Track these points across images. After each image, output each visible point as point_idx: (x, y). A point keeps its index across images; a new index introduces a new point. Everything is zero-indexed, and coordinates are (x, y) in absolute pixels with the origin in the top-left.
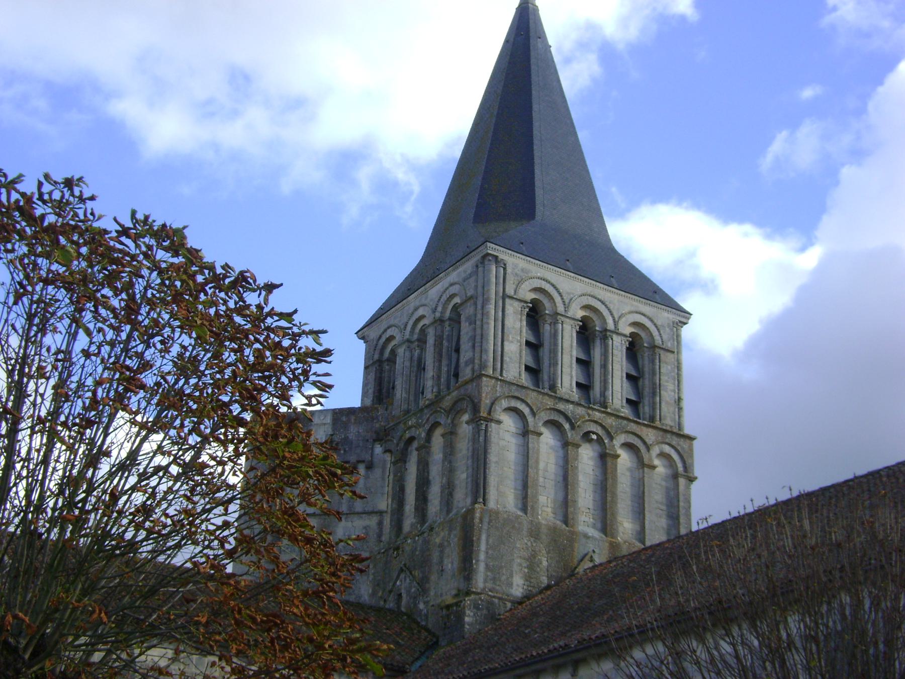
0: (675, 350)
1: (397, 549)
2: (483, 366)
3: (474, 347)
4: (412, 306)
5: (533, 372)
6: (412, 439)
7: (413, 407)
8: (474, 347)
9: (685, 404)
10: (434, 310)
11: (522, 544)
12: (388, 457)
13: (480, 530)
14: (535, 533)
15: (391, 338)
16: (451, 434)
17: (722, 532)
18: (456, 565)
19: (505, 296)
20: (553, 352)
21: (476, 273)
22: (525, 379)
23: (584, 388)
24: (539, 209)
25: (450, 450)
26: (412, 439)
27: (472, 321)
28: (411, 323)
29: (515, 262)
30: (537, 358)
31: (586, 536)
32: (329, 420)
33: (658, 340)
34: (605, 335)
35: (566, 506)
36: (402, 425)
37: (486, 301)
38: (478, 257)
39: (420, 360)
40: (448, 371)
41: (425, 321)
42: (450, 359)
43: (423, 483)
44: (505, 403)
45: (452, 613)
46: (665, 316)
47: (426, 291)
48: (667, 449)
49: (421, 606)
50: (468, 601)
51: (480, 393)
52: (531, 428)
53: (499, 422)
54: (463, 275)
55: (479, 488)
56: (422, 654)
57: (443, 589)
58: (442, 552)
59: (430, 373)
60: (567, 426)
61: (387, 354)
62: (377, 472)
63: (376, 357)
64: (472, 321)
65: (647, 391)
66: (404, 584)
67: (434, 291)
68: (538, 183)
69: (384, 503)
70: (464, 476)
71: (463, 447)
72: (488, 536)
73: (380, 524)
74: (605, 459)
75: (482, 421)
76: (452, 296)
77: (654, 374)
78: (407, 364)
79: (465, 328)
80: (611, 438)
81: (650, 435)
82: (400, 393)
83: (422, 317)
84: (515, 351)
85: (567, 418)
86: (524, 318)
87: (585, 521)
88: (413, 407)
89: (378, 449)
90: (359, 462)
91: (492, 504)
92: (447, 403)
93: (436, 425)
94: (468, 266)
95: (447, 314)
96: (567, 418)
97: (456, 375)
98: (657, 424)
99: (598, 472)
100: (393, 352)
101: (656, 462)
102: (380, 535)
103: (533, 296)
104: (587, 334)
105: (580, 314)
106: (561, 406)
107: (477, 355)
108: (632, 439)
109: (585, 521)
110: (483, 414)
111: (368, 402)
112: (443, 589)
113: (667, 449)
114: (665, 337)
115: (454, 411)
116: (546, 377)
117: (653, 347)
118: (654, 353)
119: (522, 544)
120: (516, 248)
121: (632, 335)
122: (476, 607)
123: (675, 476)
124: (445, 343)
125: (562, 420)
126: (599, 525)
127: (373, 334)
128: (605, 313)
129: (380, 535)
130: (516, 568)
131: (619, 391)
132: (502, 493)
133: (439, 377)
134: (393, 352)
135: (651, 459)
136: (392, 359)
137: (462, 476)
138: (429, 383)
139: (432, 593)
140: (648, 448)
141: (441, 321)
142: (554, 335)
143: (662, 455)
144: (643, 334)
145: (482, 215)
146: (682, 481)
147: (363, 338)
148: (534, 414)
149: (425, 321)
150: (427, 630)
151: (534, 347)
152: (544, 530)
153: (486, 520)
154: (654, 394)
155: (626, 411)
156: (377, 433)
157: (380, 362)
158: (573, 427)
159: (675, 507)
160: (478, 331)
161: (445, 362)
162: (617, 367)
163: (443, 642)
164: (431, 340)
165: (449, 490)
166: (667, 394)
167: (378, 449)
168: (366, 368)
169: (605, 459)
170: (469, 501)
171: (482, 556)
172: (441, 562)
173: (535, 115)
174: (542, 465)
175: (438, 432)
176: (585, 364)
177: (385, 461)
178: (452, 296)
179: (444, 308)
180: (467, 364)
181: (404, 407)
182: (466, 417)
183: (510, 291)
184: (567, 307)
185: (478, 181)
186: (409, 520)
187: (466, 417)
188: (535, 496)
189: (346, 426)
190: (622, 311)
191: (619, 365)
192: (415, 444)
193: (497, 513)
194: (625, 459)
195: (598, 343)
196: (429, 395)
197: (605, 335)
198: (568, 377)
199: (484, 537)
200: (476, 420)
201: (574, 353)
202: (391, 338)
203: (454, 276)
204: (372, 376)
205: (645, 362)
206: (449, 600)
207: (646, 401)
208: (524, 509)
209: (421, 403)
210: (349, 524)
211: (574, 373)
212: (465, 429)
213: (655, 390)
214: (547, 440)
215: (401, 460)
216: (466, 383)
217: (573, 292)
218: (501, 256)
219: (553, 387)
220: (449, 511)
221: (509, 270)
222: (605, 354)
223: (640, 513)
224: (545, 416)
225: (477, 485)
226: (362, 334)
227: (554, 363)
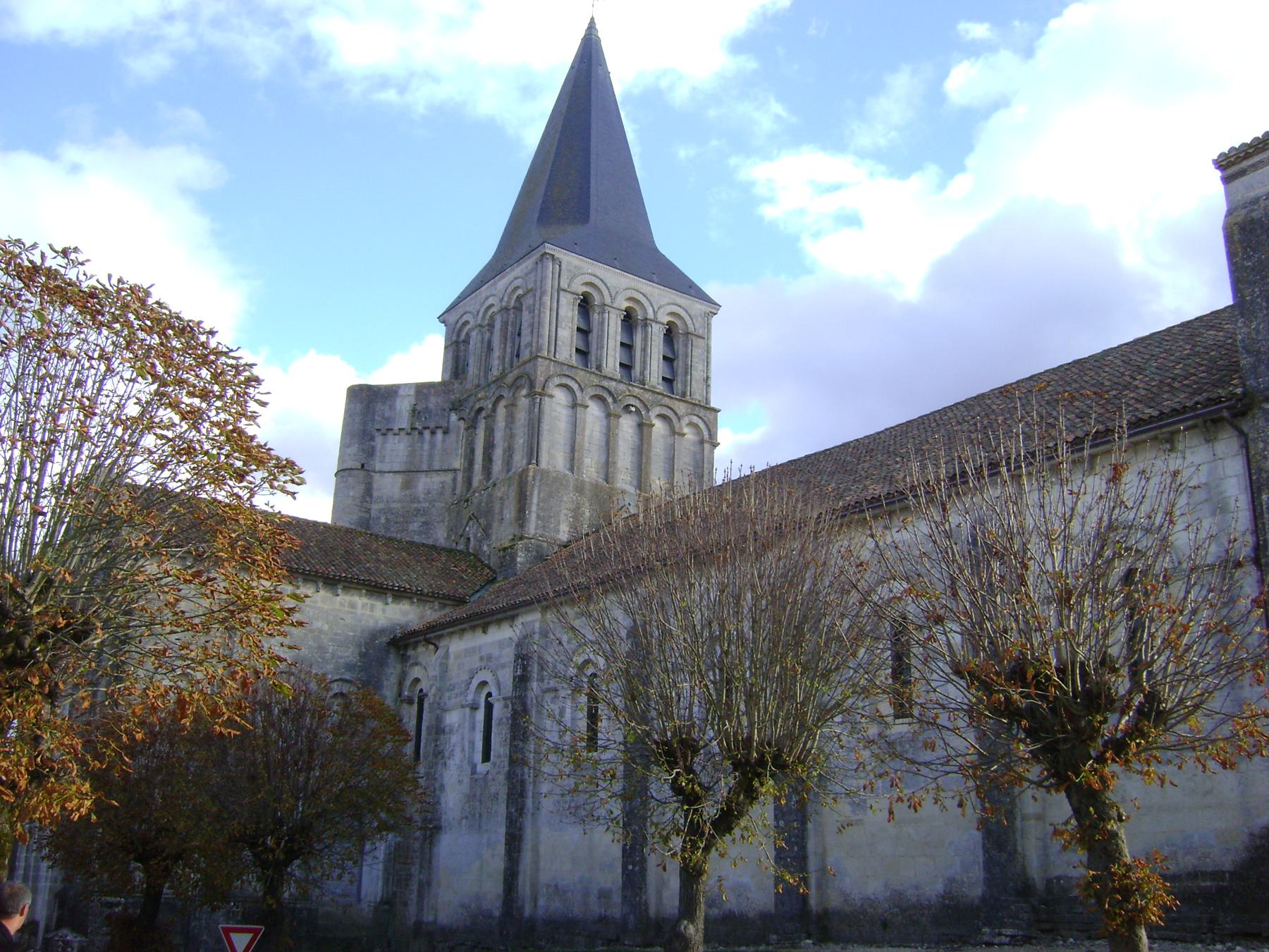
0: (706, 337)
1: (467, 501)
2: (539, 349)
3: (532, 332)
4: (484, 296)
5: (583, 353)
6: (481, 409)
7: (483, 382)
8: (532, 332)
9: (713, 382)
10: (502, 300)
11: (568, 499)
12: (462, 424)
13: (533, 486)
14: (579, 489)
15: (467, 323)
16: (512, 405)
17: (739, 486)
18: (513, 515)
19: (559, 289)
20: (601, 337)
21: (536, 269)
22: (574, 360)
23: (626, 367)
24: (592, 217)
25: (511, 419)
26: (481, 409)
27: (532, 311)
28: (482, 310)
29: (570, 260)
30: (587, 343)
31: (623, 492)
32: (412, 392)
33: (691, 329)
34: (646, 322)
36: (473, 398)
37: (543, 293)
38: (538, 255)
39: (490, 342)
40: (512, 352)
41: (494, 309)
42: (513, 343)
43: (489, 446)
44: (557, 381)
45: (507, 553)
47: (495, 284)
48: (695, 419)
49: (485, 548)
50: (520, 544)
51: (535, 371)
52: (579, 402)
53: (551, 396)
55: (533, 452)
56: (482, 587)
57: (502, 534)
58: (502, 504)
59: (497, 353)
60: (610, 400)
61: (463, 334)
62: (452, 437)
63: (454, 338)
64: (532, 311)
65: (680, 371)
66: (472, 530)
67: (502, 283)
68: (593, 190)
69: (458, 463)
70: (521, 441)
71: (521, 416)
72: (539, 492)
74: (643, 427)
75: (537, 395)
76: (516, 288)
77: (687, 356)
78: (479, 345)
79: (526, 316)
80: (648, 410)
81: (681, 408)
82: (472, 370)
83: (492, 305)
84: (567, 336)
85: (610, 393)
86: (576, 308)
87: (624, 479)
88: (483, 382)
89: (454, 417)
91: (543, 465)
92: (510, 379)
93: (500, 397)
94: (529, 263)
95: (512, 303)
96: (610, 393)
97: (518, 356)
98: (688, 398)
99: (636, 439)
100: (468, 335)
101: (686, 430)
102: (454, 490)
103: (585, 289)
104: (629, 321)
105: (625, 305)
106: (605, 383)
107: (535, 340)
109: (624, 479)
110: (538, 389)
111: (447, 377)
112: (502, 534)
113: (695, 419)
114: (697, 325)
115: (515, 386)
116: (593, 358)
117: (687, 334)
118: (687, 339)
119: (568, 499)
120: (572, 247)
121: (669, 323)
122: (527, 550)
123: (702, 442)
125: (606, 395)
126: (635, 482)
127: (452, 319)
128: (646, 304)
129: (454, 490)
130: (562, 517)
131: (655, 370)
132: (554, 456)
133: (504, 358)
134: (468, 335)
135: (681, 428)
136: (466, 342)
137: (520, 441)
138: (496, 362)
140: (679, 419)
141: (506, 309)
142: (602, 323)
143: (691, 424)
144: (678, 323)
145: (545, 217)
146: (707, 446)
147: (443, 322)
148: (582, 390)
149: (494, 309)
150: (489, 568)
151: (584, 332)
152: (588, 487)
153: (538, 478)
154: (686, 373)
155: (661, 388)
156: (453, 404)
157: (457, 342)
158: (615, 401)
159: (702, 465)
160: (536, 319)
161: (509, 345)
162: (655, 350)
163: (500, 579)
164: (498, 326)
165: (509, 451)
166: (698, 374)
167: (454, 417)
168: (446, 348)
169: (643, 427)
170: (525, 462)
171: (534, 508)
172: (501, 512)
173: (593, 132)
174: (587, 432)
175: (502, 403)
176: (627, 347)
177: (459, 428)
178: (516, 288)
179: (510, 298)
180: (526, 347)
181: (476, 382)
182: (524, 392)
183: (564, 285)
184: (613, 299)
185: (542, 190)
186: (477, 478)
187: (524, 392)
188: (581, 459)
189: (427, 397)
190: (661, 303)
191: (657, 347)
192: (484, 414)
193: (548, 472)
194: (659, 427)
195: (639, 329)
196: (496, 372)
197: (646, 322)
198: (612, 359)
199: (536, 492)
200: (532, 395)
201: (619, 338)
202: (467, 323)
203: (518, 271)
204: (450, 355)
205: (679, 346)
206: (507, 545)
207: (679, 378)
208: (572, 469)
209: (491, 378)
210: (428, 480)
211: (618, 355)
212: (523, 402)
213: (688, 370)
214: (594, 411)
215: (472, 426)
216: (525, 363)
217: (619, 287)
218: (557, 255)
219: (599, 367)
220: (508, 471)
221: (563, 267)
222: (645, 339)
223: (671, 472)
224: (591, 392)
225: (532, 449)
227: (600, 347)
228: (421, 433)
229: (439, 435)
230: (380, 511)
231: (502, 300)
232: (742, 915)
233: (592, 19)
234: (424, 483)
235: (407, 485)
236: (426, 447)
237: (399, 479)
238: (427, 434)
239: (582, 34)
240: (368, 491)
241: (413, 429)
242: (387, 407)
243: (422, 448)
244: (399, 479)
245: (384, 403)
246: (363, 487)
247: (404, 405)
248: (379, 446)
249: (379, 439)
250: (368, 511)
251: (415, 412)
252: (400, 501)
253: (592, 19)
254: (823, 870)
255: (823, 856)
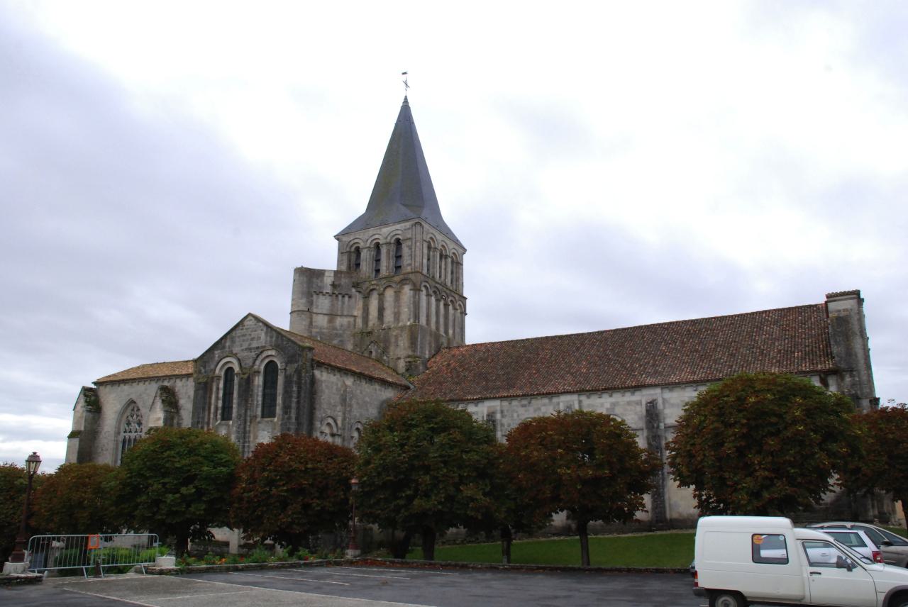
3: (411, 259)
32: (332, 275)
35: (437, 328)
36: (367, 283)
46: (461, 251)
54: (404, 228)
62: (353, 300)
73: (355, 321)
77: (457, 273)
89: (354, 290)
90: (347, 294)
106: (437, 285)
107: (413, 263)
108: (453, 299)
124: (391, 253)
127: (345, 239)
139: (391, 353)
147: (338, 239)
156: (353, 283)
160: (413, 253)
189: (340, 278)
210: (341, 320)
215: (367, 297)
218: (423, 223)
224: (433, 289)
226: (337, 237)
228: (337, 296)
229: (346, 298)
230: (317, 333)
231: (386, 238)
232: (59, 469)
233: (406, 97)
234: (339, 321)
235: (331, 321)
236: (340, 303)
237: (326, 318)
238: (340, 297)
239: (401, 104)
240: (311, 323)
241: (333, 293)
242: (319, 281)
243: (337, 304)
244: (326, 318)
245: (317, 279)
246: (309, 320)
247: (328, 280)
248: (315, 300)
249: (315, 296)
250: (311, 332)
251: (334, 285)
252: (327, 328)
253: (406, 97)
254: (670, 505)
255: (670, 499)
